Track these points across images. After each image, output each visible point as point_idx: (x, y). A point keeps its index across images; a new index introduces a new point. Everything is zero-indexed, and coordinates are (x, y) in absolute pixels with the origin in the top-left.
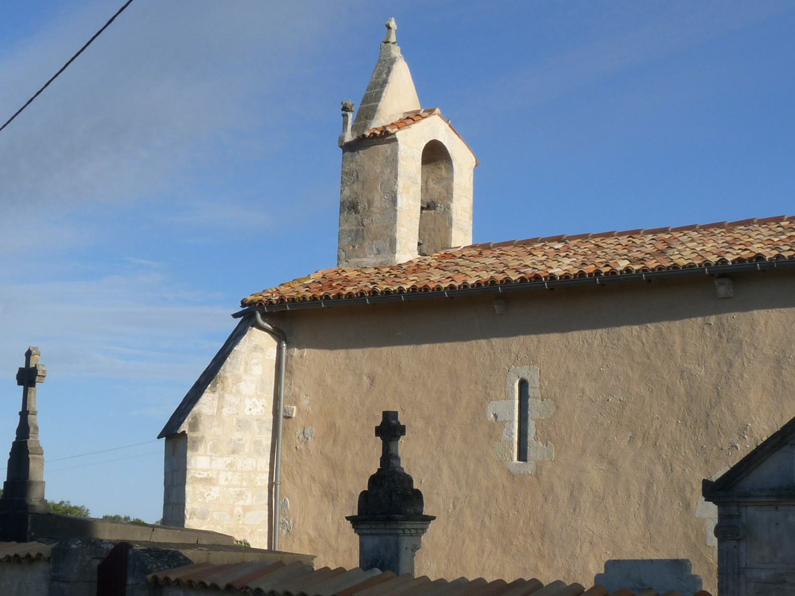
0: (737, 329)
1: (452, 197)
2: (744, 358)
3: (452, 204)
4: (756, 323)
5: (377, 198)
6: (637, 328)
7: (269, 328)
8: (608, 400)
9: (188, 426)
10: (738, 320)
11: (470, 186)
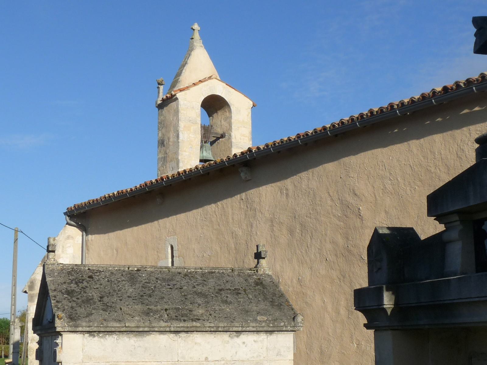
0: (420, 191)
1: (232, 128)
2: (257, 221)
3: (232, 133)
4: (261, 196)
5: (171, 136)
6: (214, 206)
7: (74, 224)
8: (204, 256)
9: (28, 287)
10: (253, 193)
11: (249, 120)
